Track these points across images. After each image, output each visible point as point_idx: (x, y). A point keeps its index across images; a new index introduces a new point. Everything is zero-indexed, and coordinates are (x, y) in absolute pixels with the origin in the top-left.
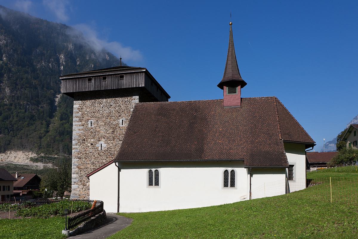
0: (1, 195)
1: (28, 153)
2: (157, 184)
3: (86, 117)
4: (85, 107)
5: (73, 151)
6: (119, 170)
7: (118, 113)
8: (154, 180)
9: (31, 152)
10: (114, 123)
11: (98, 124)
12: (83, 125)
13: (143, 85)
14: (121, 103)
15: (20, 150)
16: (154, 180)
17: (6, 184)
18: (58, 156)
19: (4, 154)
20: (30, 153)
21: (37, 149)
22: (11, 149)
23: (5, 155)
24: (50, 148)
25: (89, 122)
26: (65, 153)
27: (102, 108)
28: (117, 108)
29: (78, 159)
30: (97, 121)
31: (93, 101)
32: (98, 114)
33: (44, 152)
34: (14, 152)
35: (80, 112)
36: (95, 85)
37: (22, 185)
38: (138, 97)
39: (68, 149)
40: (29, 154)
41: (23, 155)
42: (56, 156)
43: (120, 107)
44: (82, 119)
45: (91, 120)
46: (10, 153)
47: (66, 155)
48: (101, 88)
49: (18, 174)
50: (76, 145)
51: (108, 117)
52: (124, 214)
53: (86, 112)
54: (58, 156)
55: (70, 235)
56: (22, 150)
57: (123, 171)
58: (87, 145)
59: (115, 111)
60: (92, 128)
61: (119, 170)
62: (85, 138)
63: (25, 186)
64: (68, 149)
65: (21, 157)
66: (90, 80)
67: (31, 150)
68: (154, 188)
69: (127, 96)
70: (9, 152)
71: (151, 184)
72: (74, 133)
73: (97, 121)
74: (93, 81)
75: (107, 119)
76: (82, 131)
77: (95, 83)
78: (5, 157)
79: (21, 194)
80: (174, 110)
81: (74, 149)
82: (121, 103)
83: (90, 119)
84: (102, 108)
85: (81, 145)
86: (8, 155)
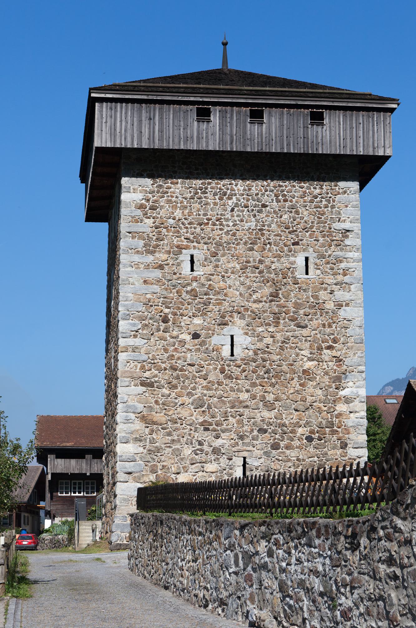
12: (161, 267)
25: (185, 257)
31: (198, 183)
35: (147, 221)
50: (135, 336)
60: (195, 279)
75: (251, 249)
77: (222, 129)
83: (187, 248)
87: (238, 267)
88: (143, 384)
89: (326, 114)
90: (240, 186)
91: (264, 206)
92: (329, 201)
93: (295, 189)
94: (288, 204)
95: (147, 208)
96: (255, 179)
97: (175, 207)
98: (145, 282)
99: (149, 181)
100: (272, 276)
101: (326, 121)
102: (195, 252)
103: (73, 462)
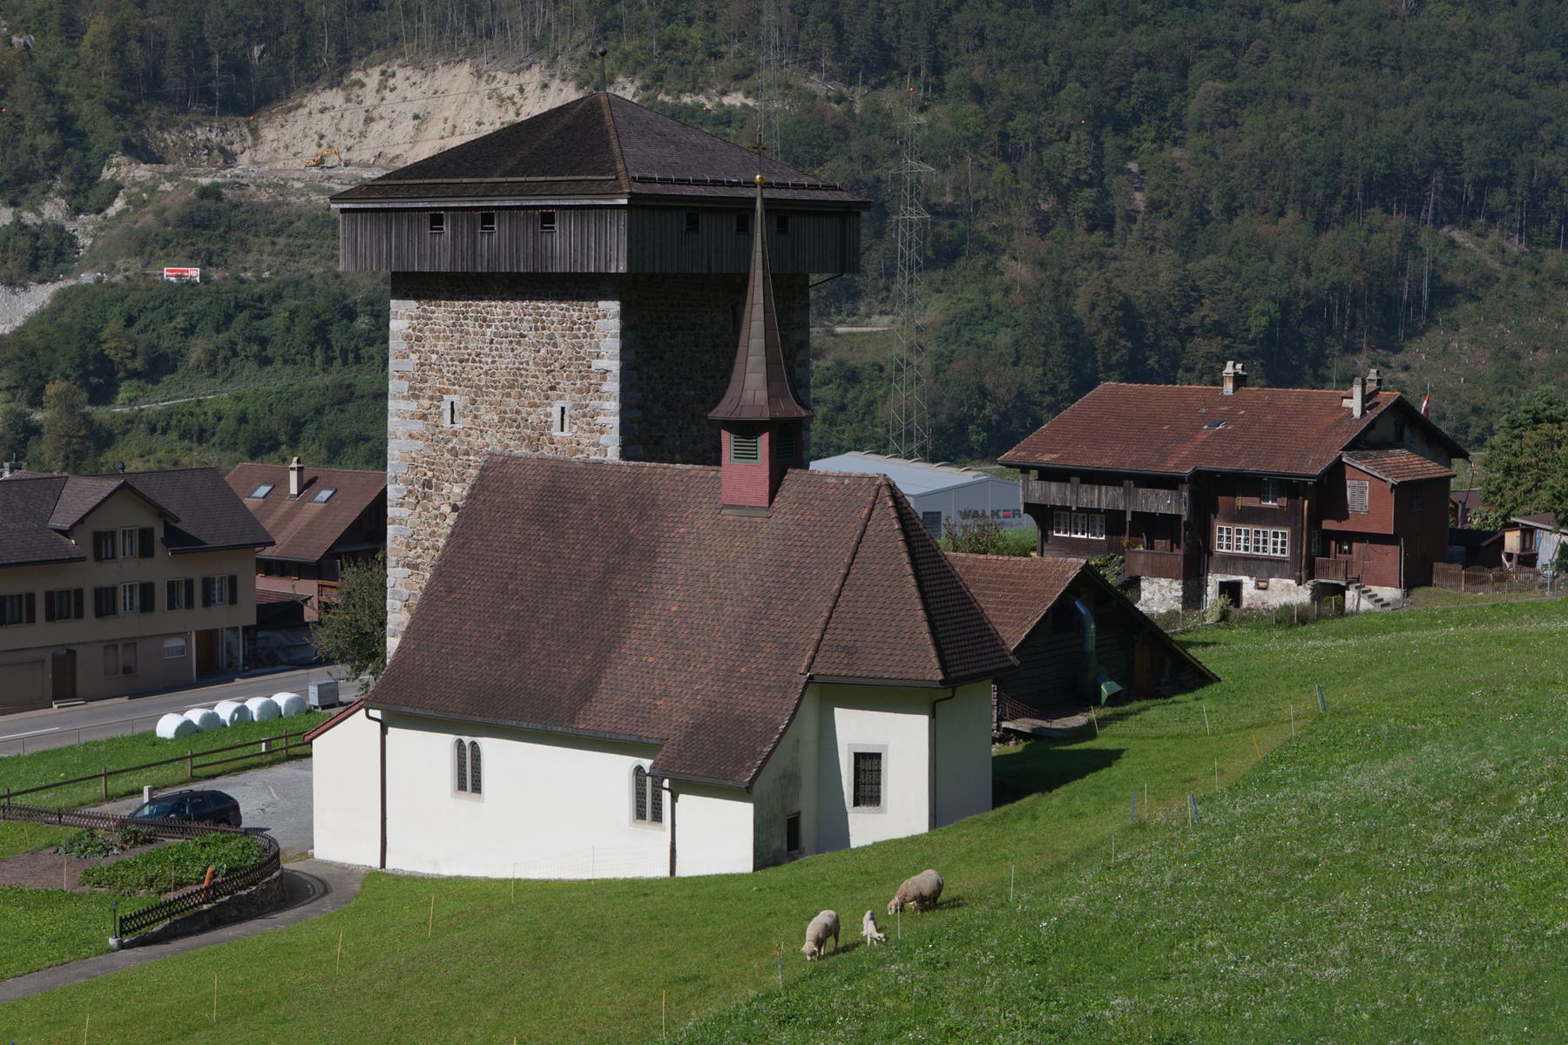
0: (197, 633)
1: (515, 81)
2: (477, 788)
3: (435, 382)
4: (432, 330)
5: (390, 529)
6: (384, 732)
7: (548, 372)
8: (469, 777)
9: (536, 69)
10: (533, 419)
11: (476, 417)
12: (424, 417)
13: (622, 269)
14: (556, 329)
15: (453, 60)
16: (469, 777)
17: (218, 570)
18: (750, 102)
19: (334, 98)
20: (533, 77)
21: (580, 35)
22: (390, 46)
23: (348, 100)
24: (690, 22)
25: (446, 406)
26: (815, 68)
27: (491, 342)
28: (543, 351)
29: (409, 571)
30: (474, 402)
31: (459, 305)
32: (475, 372)
33: (638, 63)
34: (409, 71)
35: (412, 356)
36: (454, 246)
37: (314, 551)
38: (613, 306)
39: (838, 27)
40: (521, 90)
41: (475, 103)
42: (735, 100)
43: (555, 345)
44: (421, 390)
45: (455, 398)
46: (382, 86)
47: (817, 85)
48: (475, 265)
49: (300, 470)
50: (402, 505)
51: (512, 387)
52: (398, 879)
53: (434, 357)
54: (750, 102)
55: (122, 946)
56: (472, 53)
57: (393, 732)
58: (438, 508)
59: (537, 364)
60: (455, 434)
61: (384, 732)
62: (430, 474)
63: (332, 554)
64: (838, 27)
65: (466, 113)
66: (436, 219)
67: (540, 47)
68: (466, 801)
69: (580, 297)
70: (373, 78)
71: (462, 786)
72: (394, 450)
73: (474, 402)
74: (447, 228)
75: (509, 395)
76: (420, 444)
77: (454, 238)
78: (345, 125)
79: (310, 614)
80: (582, 500)
81: (394, 522)
82: (556, 329)
83: (448, 392)
84: (491, 342)
85: (419, 509)
86: (370, 96)
87: (496, 418)
88: (408, 566)
89: (557, 213)
90: (497, 308)
91: (522, 336)
92: (588, 329)
93: (554, 310)
94: (546, 332)
95: (414, 340)
96: (513, 300)
97: (437, 338)
98: (411, 436)
99: (413, 304)
100: (529, 432)
101: (556, 226)
102: (455, 398)
103: (1054, 486)
